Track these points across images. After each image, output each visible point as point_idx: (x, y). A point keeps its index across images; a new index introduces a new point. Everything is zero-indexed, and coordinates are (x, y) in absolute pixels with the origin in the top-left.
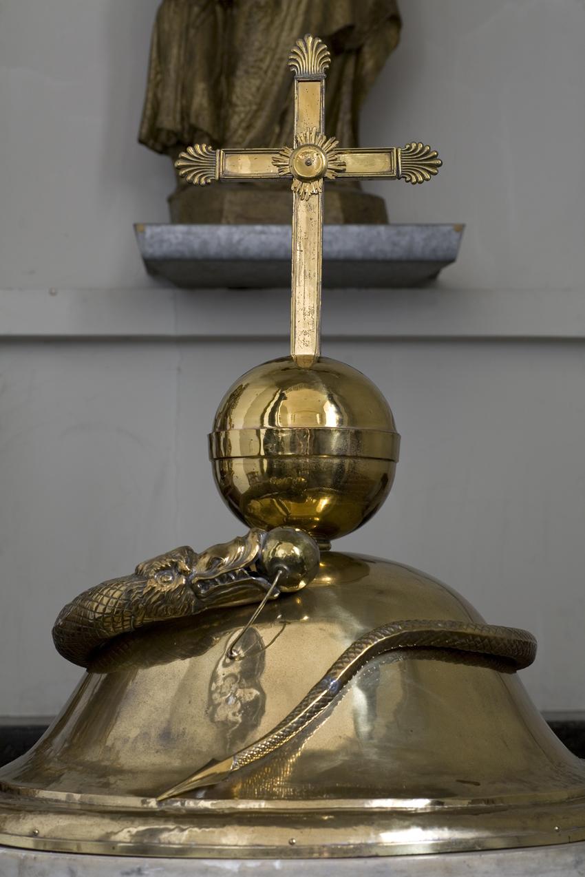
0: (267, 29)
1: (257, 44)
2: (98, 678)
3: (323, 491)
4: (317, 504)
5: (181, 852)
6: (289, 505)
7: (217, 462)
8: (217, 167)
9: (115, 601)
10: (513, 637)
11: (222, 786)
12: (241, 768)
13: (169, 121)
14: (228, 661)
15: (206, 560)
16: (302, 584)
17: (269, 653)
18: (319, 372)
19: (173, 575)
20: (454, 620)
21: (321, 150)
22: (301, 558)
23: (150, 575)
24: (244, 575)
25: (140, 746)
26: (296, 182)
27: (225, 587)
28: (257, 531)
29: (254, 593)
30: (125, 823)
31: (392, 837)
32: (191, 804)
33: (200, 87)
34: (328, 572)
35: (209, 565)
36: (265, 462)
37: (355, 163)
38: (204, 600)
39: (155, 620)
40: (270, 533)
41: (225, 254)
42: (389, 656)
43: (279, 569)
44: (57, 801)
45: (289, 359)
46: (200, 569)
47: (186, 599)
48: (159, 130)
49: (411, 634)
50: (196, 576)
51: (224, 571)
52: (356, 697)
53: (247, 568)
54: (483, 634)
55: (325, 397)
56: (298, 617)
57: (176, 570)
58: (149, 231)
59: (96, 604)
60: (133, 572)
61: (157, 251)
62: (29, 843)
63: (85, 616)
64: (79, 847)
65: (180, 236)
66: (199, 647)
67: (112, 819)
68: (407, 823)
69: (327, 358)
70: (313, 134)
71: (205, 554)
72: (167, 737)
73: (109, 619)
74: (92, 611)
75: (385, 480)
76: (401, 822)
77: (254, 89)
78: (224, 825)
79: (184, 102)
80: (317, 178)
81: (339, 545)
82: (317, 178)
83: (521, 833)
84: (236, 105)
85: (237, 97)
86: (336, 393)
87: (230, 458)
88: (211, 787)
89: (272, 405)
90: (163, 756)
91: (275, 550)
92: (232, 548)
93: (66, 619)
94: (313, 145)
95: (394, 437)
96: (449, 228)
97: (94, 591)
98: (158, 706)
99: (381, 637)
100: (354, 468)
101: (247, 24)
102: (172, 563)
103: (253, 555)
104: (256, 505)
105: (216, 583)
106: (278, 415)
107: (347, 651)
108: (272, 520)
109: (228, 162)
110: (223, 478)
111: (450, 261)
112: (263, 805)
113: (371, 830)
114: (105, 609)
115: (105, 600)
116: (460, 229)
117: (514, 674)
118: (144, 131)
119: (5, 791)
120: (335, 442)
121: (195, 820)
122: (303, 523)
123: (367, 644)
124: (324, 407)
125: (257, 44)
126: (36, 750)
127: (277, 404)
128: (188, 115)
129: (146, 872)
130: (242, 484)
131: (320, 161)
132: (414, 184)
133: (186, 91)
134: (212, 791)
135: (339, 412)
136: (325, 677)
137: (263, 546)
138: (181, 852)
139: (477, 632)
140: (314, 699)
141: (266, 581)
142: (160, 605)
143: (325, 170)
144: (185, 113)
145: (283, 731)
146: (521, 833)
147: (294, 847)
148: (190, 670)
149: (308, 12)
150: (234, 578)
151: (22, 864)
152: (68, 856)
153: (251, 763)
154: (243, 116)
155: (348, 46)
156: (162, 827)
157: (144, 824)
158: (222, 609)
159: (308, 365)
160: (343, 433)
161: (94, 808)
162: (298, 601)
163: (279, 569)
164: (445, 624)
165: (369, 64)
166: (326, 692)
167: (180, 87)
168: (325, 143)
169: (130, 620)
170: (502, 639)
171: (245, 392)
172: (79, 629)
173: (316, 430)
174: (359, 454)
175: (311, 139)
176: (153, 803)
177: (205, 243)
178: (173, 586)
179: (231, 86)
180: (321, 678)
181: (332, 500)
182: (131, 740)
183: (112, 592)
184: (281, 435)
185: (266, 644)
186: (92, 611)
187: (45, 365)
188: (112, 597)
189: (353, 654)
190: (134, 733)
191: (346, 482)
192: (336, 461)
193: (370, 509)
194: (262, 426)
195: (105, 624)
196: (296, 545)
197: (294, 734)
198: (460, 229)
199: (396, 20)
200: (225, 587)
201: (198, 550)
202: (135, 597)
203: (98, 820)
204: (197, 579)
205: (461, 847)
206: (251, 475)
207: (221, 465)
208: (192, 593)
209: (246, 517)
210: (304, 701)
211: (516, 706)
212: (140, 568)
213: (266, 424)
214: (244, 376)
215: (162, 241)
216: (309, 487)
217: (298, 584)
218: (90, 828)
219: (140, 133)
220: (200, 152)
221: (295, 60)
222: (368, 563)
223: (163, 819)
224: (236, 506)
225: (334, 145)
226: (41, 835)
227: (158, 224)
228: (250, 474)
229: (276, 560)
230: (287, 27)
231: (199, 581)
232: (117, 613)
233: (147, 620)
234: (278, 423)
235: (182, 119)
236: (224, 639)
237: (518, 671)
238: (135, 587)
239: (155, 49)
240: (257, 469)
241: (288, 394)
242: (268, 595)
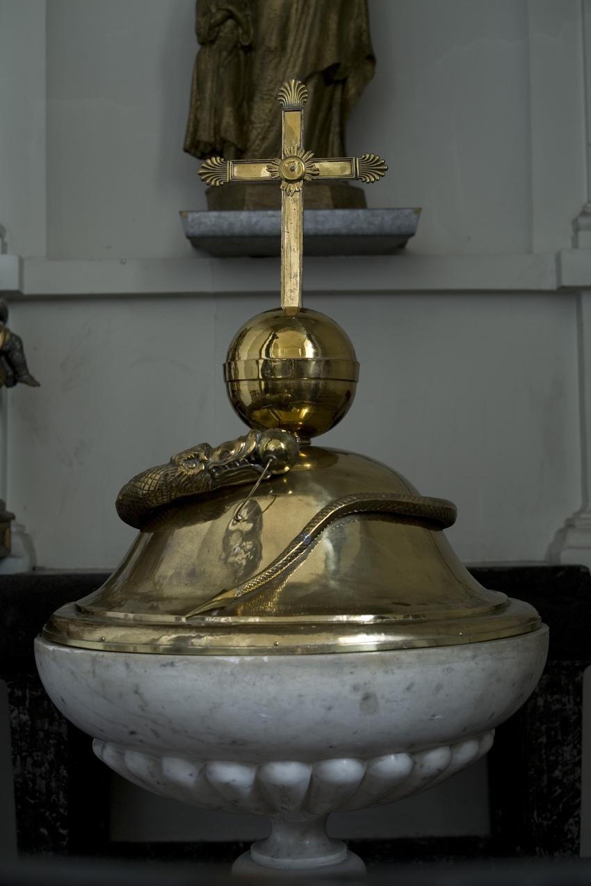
0: (276, 68)
1: (269, 78)
2: (148, 536)
3: (303, 403)
4: (300, 412)
5: (204, 651)
6: (280, 414)
7: (229, 383)
8: (228, 173)
9: (156, 482)
10: (437, 505)
11: (229, 608)
12: (243, 595)
13: (205, 136)
14: (235, 522)
15: (219, 452)
16: (287, 469)
17: (265, 515)
18: (300, 319)
19: (196, 463)
20: (394, 493)
21: (301, 159)
22: (285, 450)
23: (180, 463)
24: (245, 463)
25: (175, 582)
26: (284, 183)
27: (232, 472)
28: (254, 432)
29: (253, 476)
30: (163, 632)
31: (346, 640)
32: (209, 619)
33: (228, 110)
34: (307, 460)
35: (221, 456)
36: (263, 383)
37: (331, 168)
38: (218, 480)
39: (184, 494)
40: (264, 433)
41: (246, 232)
42: (348, 519)
43: (270, 458)
44: (118, 618)
45: (281, 309)
46: (214, 459)
47: (206, 480)
48: (199, 142)
49: (363, 503)
50: (212, 464)
51: (232, 460)
52: (325, 544)
53: (248, 457)
54: (414, 502)
55: (305, 336)
56: (285, 492)
57: (198, 460)
58: (190, 216)
59: (143, 484)
60: (169, 461)
61: (197, 231)
62: (100, 646)
63: (137, 493)
64: (135, 647)
65: (213, 219)
66: (216, 514)
67: (154, 630)
68: (356, 630)
69: (315, 311)
70: (296, 149)
71: (219, 448)
72: (193, 574)
73: (153, 495)
74: (140, 489)
75: (349, 396)
76: (352, 630)
77: (267, 111)
78: (229, 634)
79: (216, 121)
80: (298, 180)
81: (316, 442)
82: (298, 180)
83: (436, 637)
84: (254, 123)
85: (256, 117)
86: (313, 334)
87: (238, 381)
89: (267, 342)
90: (190, 588)
91: (267, 445)
92: (237, 444)
93: (124, 495)
94: (295, 157)
95: (355, 365)
96: (409, 211)
97: (143, 475)
98: (186, 553)
99: (341, 505)
100: (326, 387)
101: (262, 64)
102: (195, 455)
103: (252, 448)
104: (257, 414)
105: (226, 469)
106: (271, 350)
107: (318, 515)
108: (269, 424)
109: (236, 169)
110: (234, 396)
111: (412, 235)
112: (257, 620)
113: (331, 636)
114: (149, 488)
115: (150, 481)
116: (418, 211)
117: (439, 532)
118: (188, 143)
119: (84, 613)
120: (312, 369)
121: (210, 630)
122: (290, 427)
123: (332, 510)
124: (305, 344)
125: (269, 78)
126: (105, 586)
127: (271, 342)
128: (219, 131)
129: (177, 665)
130: (247, 399)
131: (300, 167)
132: (368, 183)
133: (217, 113)
134: (222, 611)
135: (315, 347)
136: (301, 533)
137: (259, 442)
138: (204, 651)
139: (410, 501)
140: (292, 549)
141: (260, 467)
142: (187, 484)
143: (304, 174)
144: (217, 129)
145: (272, 570)
146: (436, 637)
147: (278, 647)
148: (212, 526)
149: (306, 54)
150: (238, 465)
151: (94, 660)
152: (124, 655)
153: (250, 592)
154: (259, 130)
155: (336, 78)
156: (187, 635)
157: (175, 633)
158: (231, 486)
159: (293, 314)
160: (318, 362)
161: (143, 623)
162: (285, 481)
163: (270, 458)
164: (387, 495)
165: (352, 91)
166: (302, 543)
167: (213, 111)
168: (304, 155)
169: (167, 495)
170: (429, 506)
171: (248, 334)
172: (133, 502)
173: (298, 360)
174: (328, 377)
175: (294, 152)
176: (184, 620)
177: (231, 224)
178: (196, 471)
179: (250, 108)
180: (299, 533)
182: (168, 578)
183: (154, 475)
184: (273, 364)
185: (263, 509)
186: (140, 489)
187: (120, 315)
188: (154, 479)
189: (321, 517)
190: (170, 573)
191: (320, 397)
192: (313, 382)
193: (338, 416)
194: (261, 358)
195: (150, 498)
196: (282, 441)
197: (280, 572)
198: (418, 211)
199: (371, 58)
200: (232, 472)
201: (214, 446)
202: (170, 479)
203: (144, 631)
204: (213, 465)
205: (393, 647)
206: (253, 393)
207: (232, 386)
208: (209, 475)
209: (251, 422)
210: (286, 549)
211: (443, 555)
212: (174, 458)
213: (264, 356)
214: (251, 320)
215: (200, 224)
216: (294, 400)
217: (283, 468)
218: (143, 636)
219: (185, 145)
220: (215, 163)
221: (282, 96)
222: (339, 455)
223: (188, 630)
224: (243, 415)
225: (311, 156)
226: (107, 640)
227: (197, 212)
228: (252, 392)
229: (268, 452)
230: (291, 65)
231: (215, 467)
232: (159, 490)
233: (179, 495)
234: (272, 355)
235: (215, 134)
236: (234, 507)
238: (169, 472)
239: (195, 83)
240: (257, 388)
241: (278, 335)
242: (262, 475)
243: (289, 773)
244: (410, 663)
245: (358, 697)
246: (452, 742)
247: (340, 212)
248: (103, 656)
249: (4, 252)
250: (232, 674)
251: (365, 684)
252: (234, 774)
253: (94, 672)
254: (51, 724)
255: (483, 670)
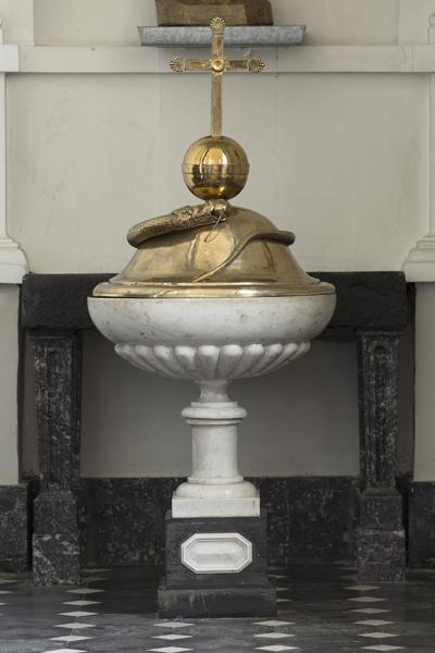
177: (173, 37)
215: (151, 36)
243: (210, 351)
245: (238, 316)
246: (284, 341)
247: (249, 28)
249: (5, 42)
252: (186, 352)
254: (60, 369)
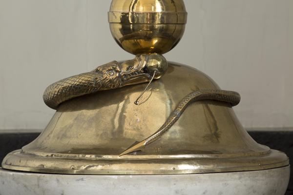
46: (124, 70)
88: (137, 151)
103: (144, 66)
105: (136, 74)
106: (135, 7)
135: (162, 5)
137: (147, 62)
178: (114, 77)
181: (152, 43)
204: (123, 74)
211: (232, 121)
213: (131, 11)
222: (174, 67)
237: (233, 107)
244: (205, 180)
248: (44, 176)
250: (114, 184)
251: (182, 190)
253: (38, 185)
255: (245, 185)
